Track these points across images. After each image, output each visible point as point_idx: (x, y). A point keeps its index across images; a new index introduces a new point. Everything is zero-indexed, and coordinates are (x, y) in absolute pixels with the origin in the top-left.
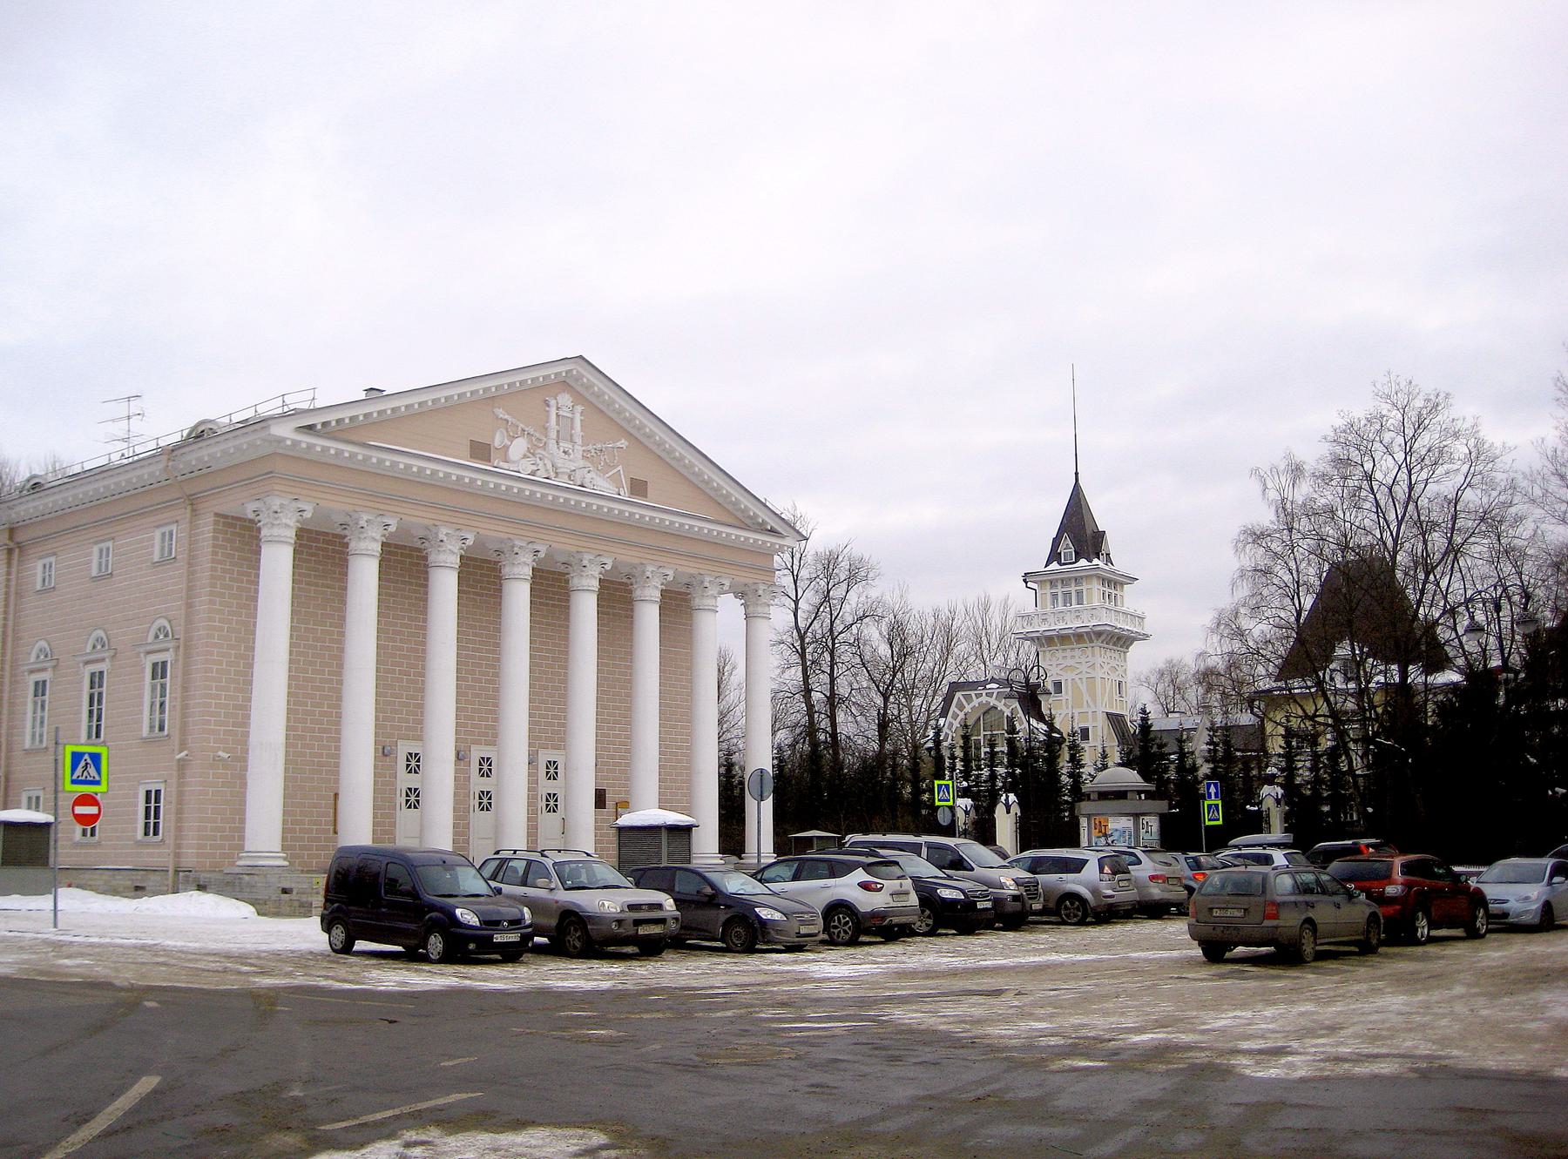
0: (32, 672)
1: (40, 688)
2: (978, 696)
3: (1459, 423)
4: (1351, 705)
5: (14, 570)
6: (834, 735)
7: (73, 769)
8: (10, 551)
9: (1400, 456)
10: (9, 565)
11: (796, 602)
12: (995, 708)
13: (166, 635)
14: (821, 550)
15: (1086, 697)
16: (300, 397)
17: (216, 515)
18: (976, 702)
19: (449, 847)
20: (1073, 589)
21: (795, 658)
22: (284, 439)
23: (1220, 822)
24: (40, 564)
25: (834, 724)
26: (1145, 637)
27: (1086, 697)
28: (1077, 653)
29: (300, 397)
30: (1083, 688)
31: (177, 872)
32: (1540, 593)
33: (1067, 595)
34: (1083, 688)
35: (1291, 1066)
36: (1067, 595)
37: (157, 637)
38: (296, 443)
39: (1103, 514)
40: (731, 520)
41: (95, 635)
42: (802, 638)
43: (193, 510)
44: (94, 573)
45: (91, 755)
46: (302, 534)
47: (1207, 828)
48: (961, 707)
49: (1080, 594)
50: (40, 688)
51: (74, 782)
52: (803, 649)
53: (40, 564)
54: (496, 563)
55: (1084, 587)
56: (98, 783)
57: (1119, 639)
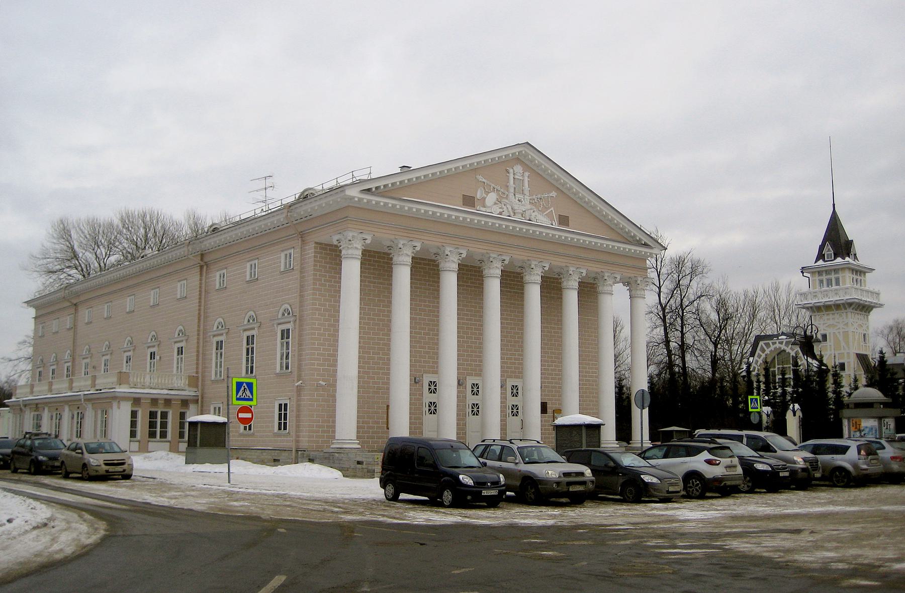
0: (214, 336)
1: (219, 345)
2: (774, 343)
5: (204, 278)
7: (237, 392)
8: (202, 267)
10: (201, 275)
11: (660, 288)
12: (784, 351)
13: (289, 314)
16: (344, 178)
17: (316, 243)
18: (772, 347)
22: (354, 197)
24: (218, 274)
26: (881, 305)
28: (837, 316)
29: (344, 178)
30: (841, 339)
31: (297, 451)
34: (841, 339)
37: (283, 315)
38: (360, 200)
39: (851, 230)
40: (619, 239)
41: (283, 307)
42: (663, 309)
43: (303, 241)
44: (248, 278)
45: (247, 383)
46: (580, 284)
48: (763, 350)
49: (837, 280)
50: (219, 345)
51: (238, 399)
52: (665, 316)
53: (218, 274)
54: (520, 274)
56: (252, 400)
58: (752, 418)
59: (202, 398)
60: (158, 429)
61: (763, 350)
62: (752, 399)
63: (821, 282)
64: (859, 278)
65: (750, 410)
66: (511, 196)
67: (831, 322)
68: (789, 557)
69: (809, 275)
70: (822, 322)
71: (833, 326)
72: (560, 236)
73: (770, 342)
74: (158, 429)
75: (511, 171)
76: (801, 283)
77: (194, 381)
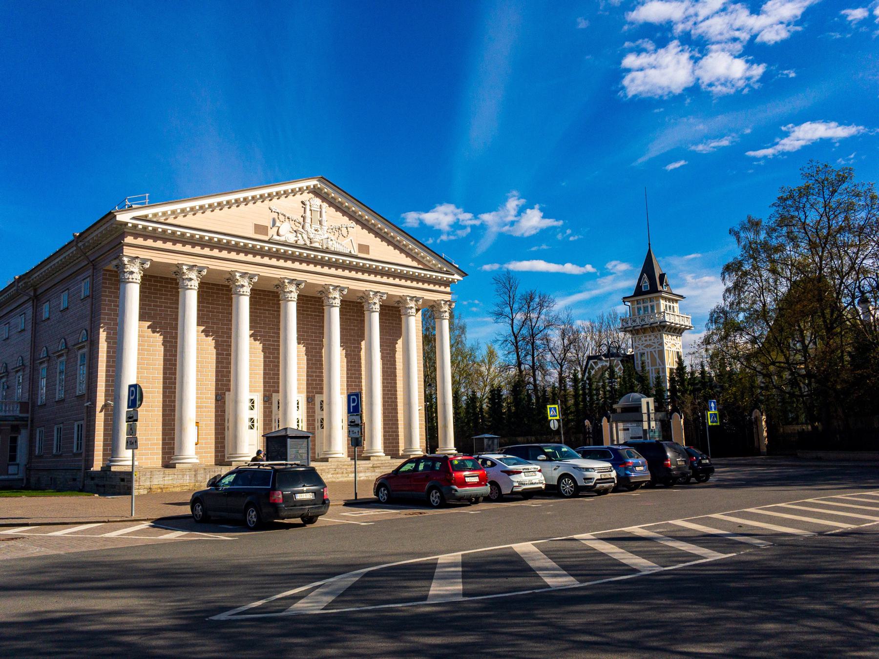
3: (860, 188)
4: (799, 357)
6: (535, 385)
9: (821, 210)
11: (512, 320)
14: (524, 293)
15: (658, 360)
18: (600, 365)
19: (305, 429)
20: (649, 304)
21: (513, 348)
22: (126, 224)
23: (548, 406)
25: (535, 380)
27: (658, 360)
30: (657, 356)
32: (130, 277)
33: (646, 309)
34: (657, 356)
35: (259, 465)
36: (646, 309)
42: (516, 338)
46: (202, 285)
47: (710, 426)
49: (652, 307)
52: (517, 343)
54: (361, 303)
55: (655, 303)
57: (676, 329)
58: (552, 426)
59: (32, 421)
62: (551, 408)
63: (639, 309)
64: (671, 304)
65: (550, 418)
66: (307, 226)
67: (648, 343)
68: (676, 602)
69: (629, 304)
70: (641, 343)
71: (650, 346)
72: (337, 260)
75: (307, 203)
76: (623, 309)
77: (24, 406)
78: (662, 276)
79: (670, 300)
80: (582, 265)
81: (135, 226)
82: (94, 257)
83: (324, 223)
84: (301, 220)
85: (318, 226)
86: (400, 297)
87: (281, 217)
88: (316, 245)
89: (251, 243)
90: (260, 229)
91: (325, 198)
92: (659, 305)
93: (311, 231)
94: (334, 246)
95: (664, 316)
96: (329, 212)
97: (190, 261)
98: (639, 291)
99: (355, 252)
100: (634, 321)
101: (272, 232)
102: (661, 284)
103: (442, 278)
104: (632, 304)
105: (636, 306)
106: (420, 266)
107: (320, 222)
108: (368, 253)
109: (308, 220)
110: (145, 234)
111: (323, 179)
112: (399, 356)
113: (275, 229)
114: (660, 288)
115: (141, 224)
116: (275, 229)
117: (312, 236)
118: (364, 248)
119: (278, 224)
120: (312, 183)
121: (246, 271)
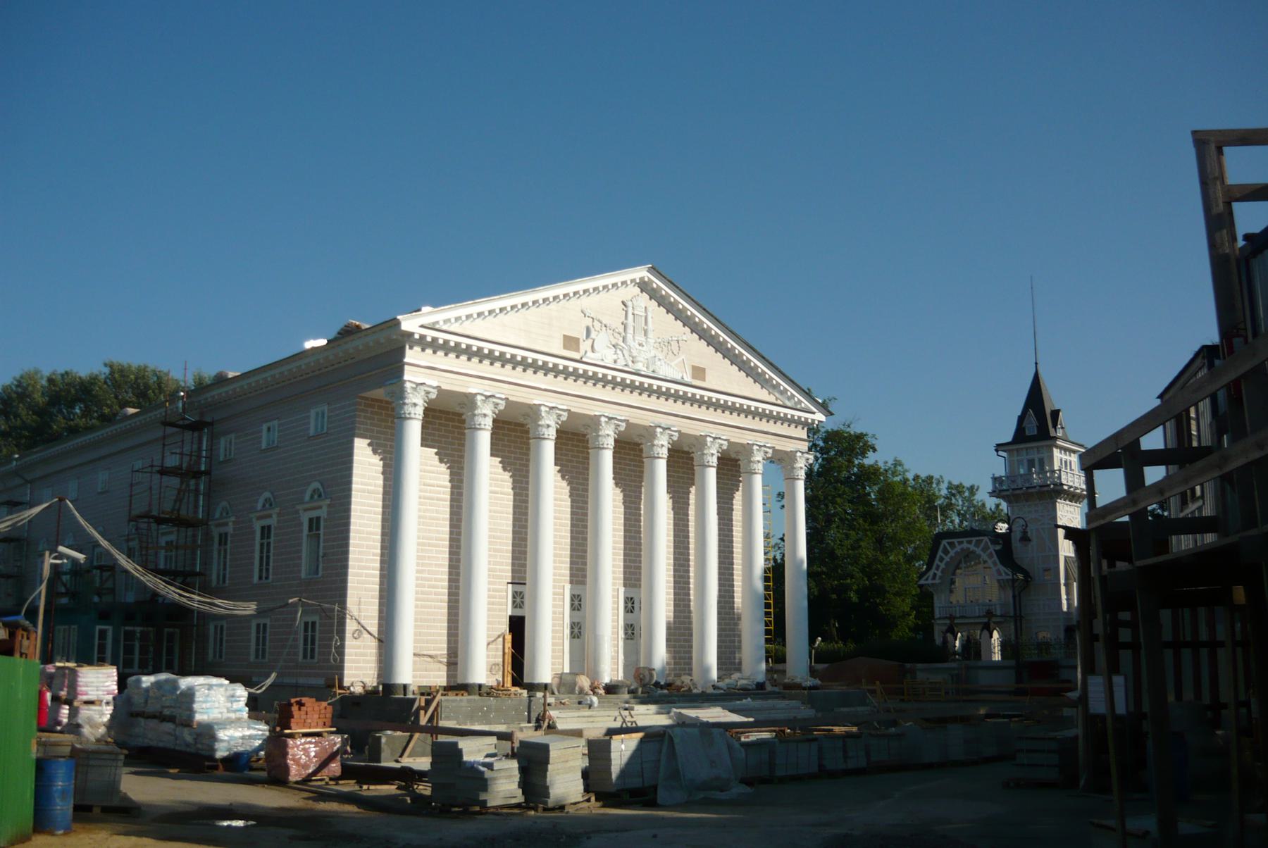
18: (958, 548)
39: (1054, 398)
49: (1042, 462)
60: (137, 656)
61: (946, 552)
64: (1068, 458)
66: (629, 336)
73: (955, 541)
74: (137, 656)
75: (629, 304)
78: (1055, 414)
79: (1066, 450)
80: (229, 826)
81: (423, 337)
82: (360, 376)
83: (651, 335)
84: (621, 329)
85: (643, 339)
86: (742, 445)
87: (597, 324)
88: (640, 366)
89: (551, 361)
90: (571, 342)
91: (654, 294)
92: (1051, 457)
93: (634, 345)
94: (664, 371)
95: (1060, 477)
96: (658, 314)
97: (552, 401)
98: (1020, 436)
99: (688, 379)
100: (1013, 481)
101: (585, 346)
102: (1055, 426)
103: (659, 288)
104: (1010, 455)
105: (1015, 458)
106: (772, 399)
107: (646, 332)
108: (704, 380)
109: (630, 330)
110: (434, 346)
111: (653, 270)
112: (737, 515)
113: (589, 342)
114: (1052, 433)
115: (430, 334)
116: (589, 342)
117: (635, 353)
118: (699, 372)
119: (593, 335)
120: (641, 273)
121: (552, 401)
